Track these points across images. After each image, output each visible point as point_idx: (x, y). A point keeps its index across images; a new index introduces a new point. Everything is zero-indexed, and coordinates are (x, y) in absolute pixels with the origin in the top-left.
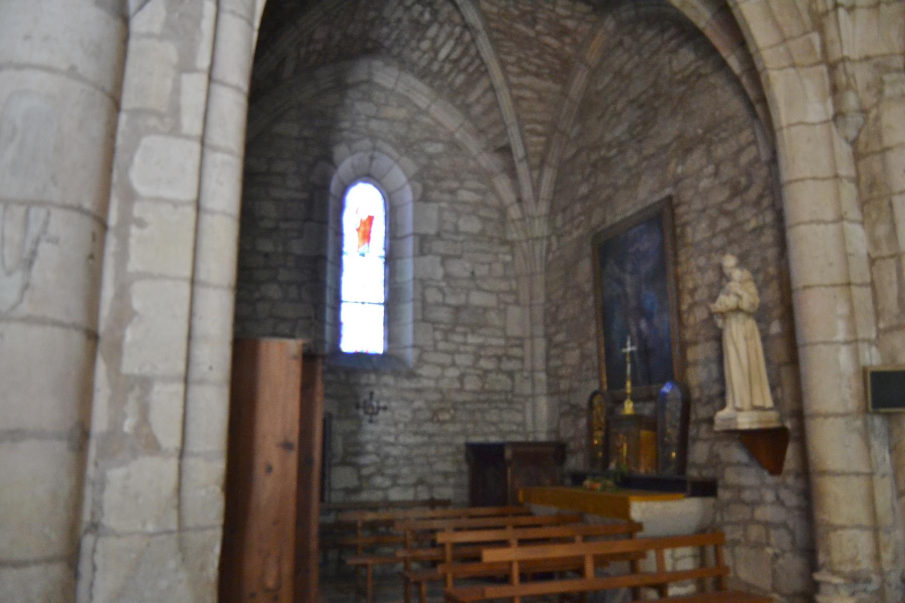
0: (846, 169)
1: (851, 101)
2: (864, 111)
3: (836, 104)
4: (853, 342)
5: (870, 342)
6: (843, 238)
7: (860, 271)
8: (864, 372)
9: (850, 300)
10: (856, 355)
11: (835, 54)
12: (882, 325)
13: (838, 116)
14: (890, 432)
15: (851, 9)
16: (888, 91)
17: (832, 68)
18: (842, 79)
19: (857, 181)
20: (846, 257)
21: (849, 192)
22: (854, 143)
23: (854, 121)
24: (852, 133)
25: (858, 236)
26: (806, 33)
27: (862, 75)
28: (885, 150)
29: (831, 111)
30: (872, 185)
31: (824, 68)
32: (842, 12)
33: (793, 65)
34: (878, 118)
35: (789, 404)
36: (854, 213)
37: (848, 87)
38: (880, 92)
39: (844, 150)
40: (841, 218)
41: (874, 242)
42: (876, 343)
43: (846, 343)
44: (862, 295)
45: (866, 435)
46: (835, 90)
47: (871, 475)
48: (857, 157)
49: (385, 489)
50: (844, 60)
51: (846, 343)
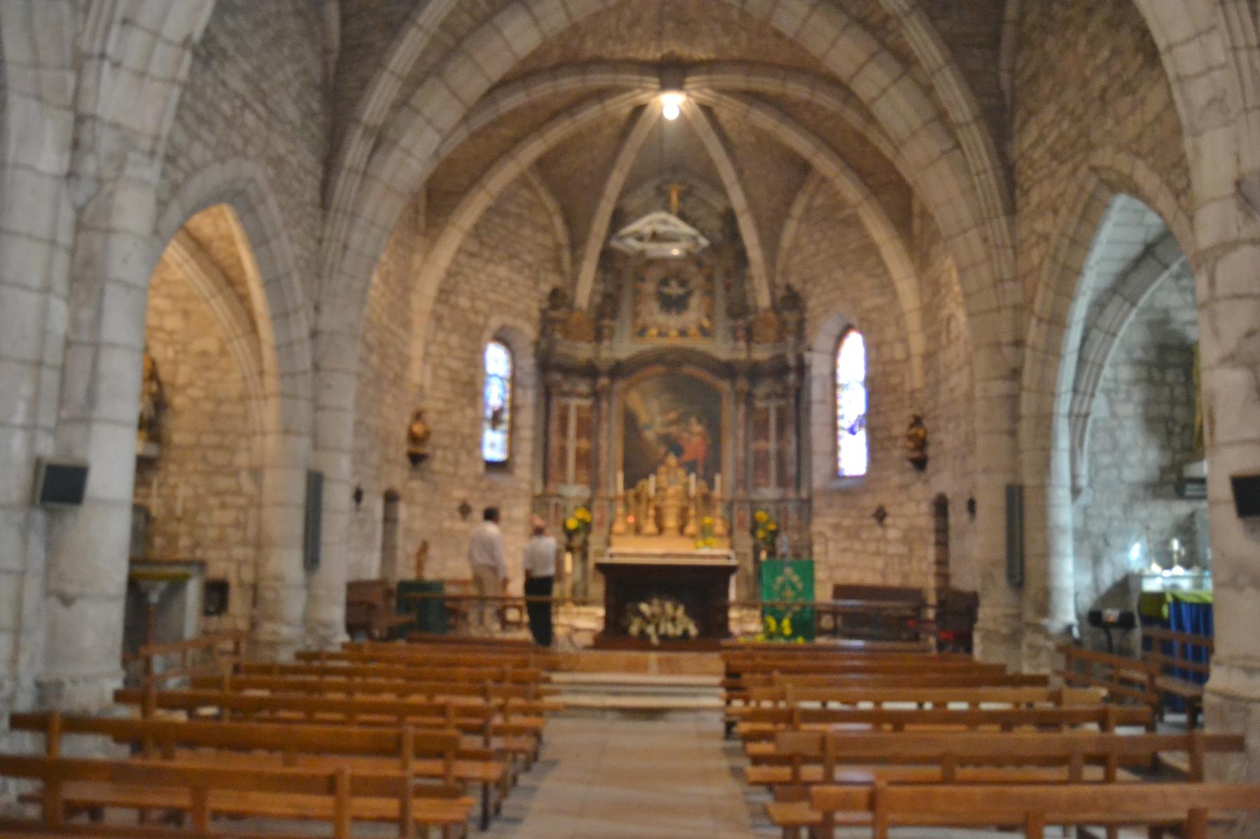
0: (65, 237)
1: (90, 165)
2: (99, 181)
3: (74, 161)
4: (31, 428)
5: (48, 430)
6: (44, 312)
7: (53, 354)
8: (38, 462)
9: (38, 382)
10: (31, 442)
11: (87, 106)
12: (64, 414)
13: (71, 175)
14: (49, 529)
15: (117, 65)
16: (129, 171)
17: (80, 120)
18: (86, 138)
19: (73, 251)
20: (44, 333)
21: (61, 262)
22: (80, 210)
23: (85, 189)
24: (81, 200)
25: (59, 312)
26: (62, 67)
27: (107, 142)
28: (109, 231)
29: (65, 167)
30: (88, 263)
31: (69, 117)
32: (107, 66)
33: (39, 98)
34: (111, 195)
35: (556, 402)
36: (61, 286)
37: (92, 149)
38: (120, 168)
39: (67, 215)
40: (47, 289)
41: (74, 323)
42: (53, 432)
43: (24, 427)
44: (50, 378)
45: (25, 530)
46: (76, 145)
47: (22, 574)
48: (79, 227)
49: (812, 197)
50: (94, 118)
51: (24, 427)
